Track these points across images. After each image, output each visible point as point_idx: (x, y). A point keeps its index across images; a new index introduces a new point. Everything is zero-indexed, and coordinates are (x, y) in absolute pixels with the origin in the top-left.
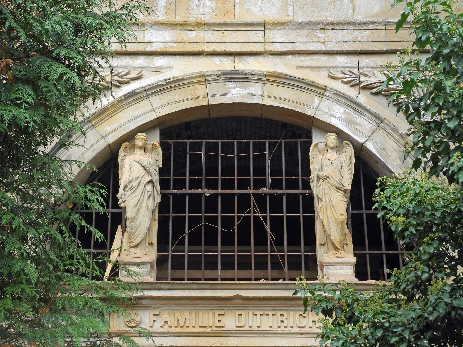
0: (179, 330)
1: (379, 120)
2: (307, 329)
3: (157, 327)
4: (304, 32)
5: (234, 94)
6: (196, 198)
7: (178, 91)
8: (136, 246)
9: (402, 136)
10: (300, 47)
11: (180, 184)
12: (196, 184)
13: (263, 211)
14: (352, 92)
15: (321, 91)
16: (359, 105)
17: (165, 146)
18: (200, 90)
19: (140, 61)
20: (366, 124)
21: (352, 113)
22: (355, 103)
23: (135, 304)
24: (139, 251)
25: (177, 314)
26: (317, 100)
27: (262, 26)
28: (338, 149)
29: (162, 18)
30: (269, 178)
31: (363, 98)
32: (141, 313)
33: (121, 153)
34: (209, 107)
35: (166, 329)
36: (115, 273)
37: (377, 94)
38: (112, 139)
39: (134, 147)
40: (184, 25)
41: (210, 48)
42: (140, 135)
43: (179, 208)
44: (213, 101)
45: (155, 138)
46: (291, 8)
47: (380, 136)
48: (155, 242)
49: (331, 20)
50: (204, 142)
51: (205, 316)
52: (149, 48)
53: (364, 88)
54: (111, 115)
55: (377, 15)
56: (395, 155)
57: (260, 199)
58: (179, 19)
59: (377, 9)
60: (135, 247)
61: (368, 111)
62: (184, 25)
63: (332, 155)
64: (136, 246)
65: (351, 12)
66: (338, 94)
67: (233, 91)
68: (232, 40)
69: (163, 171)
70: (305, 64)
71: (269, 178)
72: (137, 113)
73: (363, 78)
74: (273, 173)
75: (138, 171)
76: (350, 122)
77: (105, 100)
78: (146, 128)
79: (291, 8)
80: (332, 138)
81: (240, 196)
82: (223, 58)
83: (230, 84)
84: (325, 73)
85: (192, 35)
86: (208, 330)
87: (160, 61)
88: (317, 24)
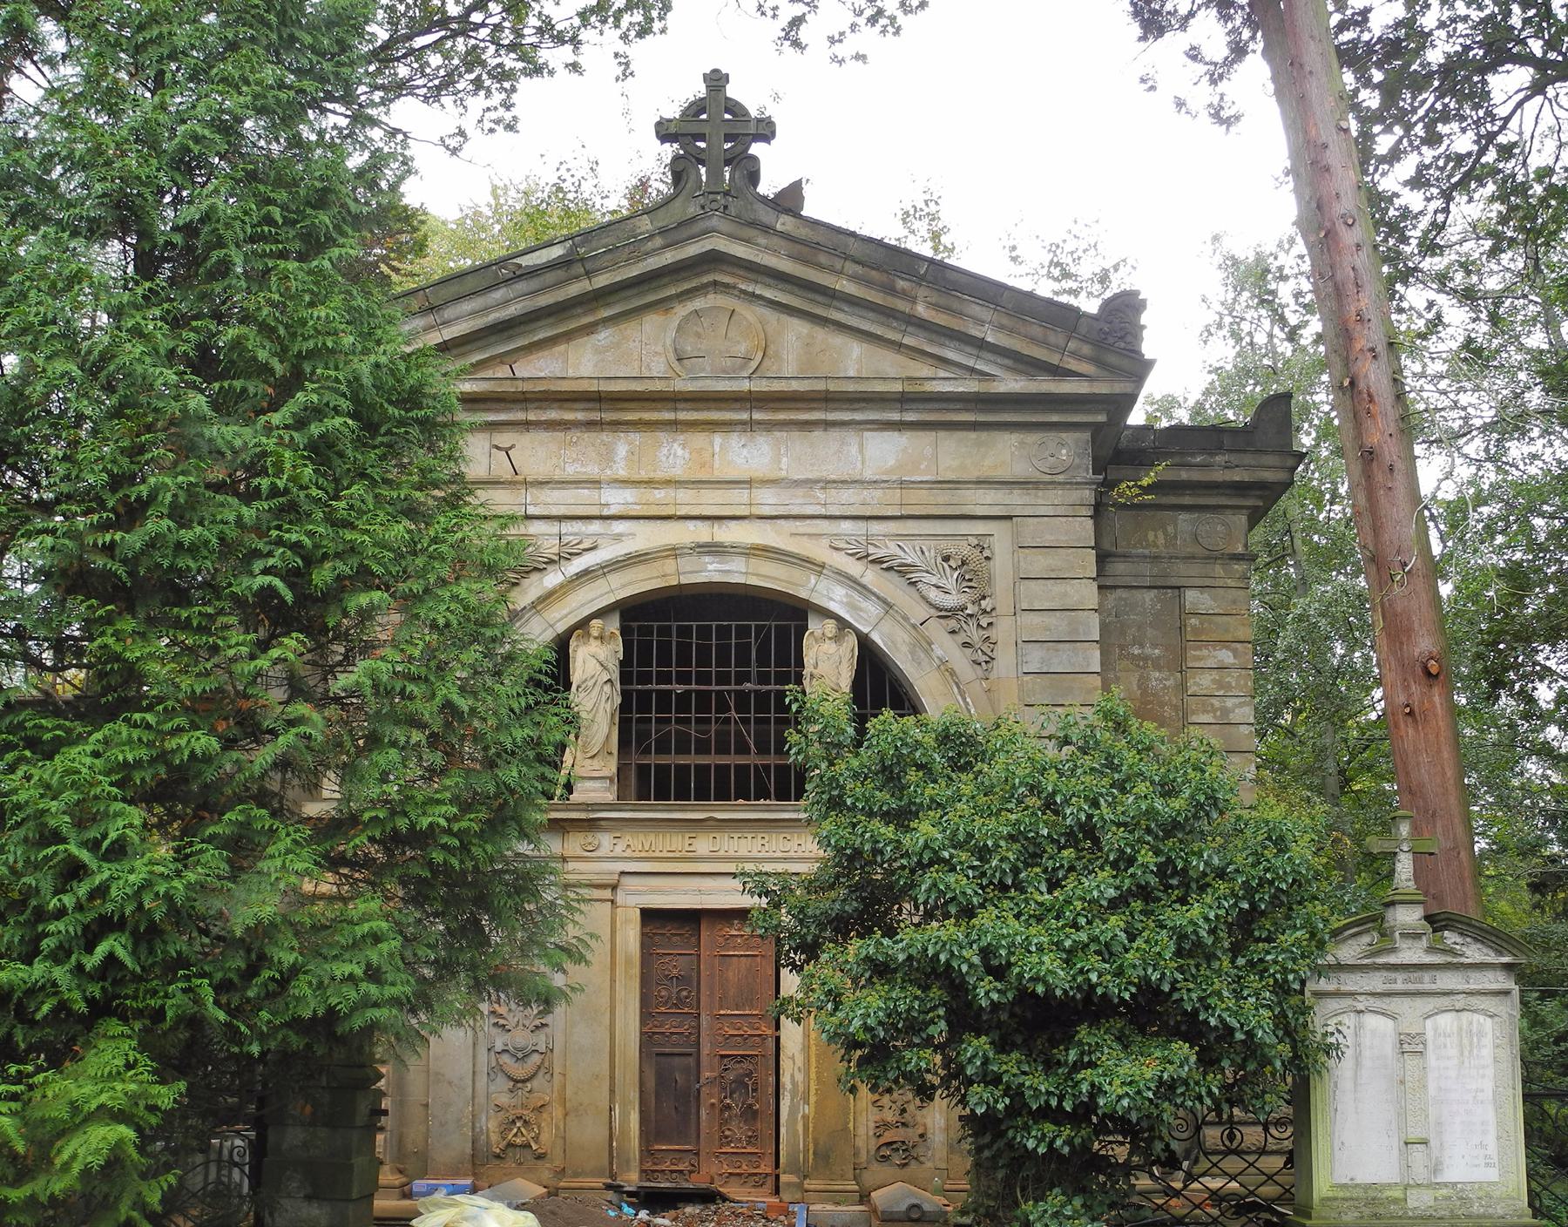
0: (643, 854)
1: (888, 605)
2: (792, 854)
3: (618, 851)
4: (800, 491)
5: (711, 571)
6: (664, 696)
7: (641, 567)
8: (593, 757)
9: (914, 626)
10: (795, 511)
11: (645, 678)
12: (664, 678)
13: (738, 733)
14: (855, 568)
15: (820, 567)
16: (864, 587)
17: (625, 631)
18: (669, 566)
19: (595, 527)
20: (872, 609)
21: (856, 596)
22: (859, 584)
23: (591, 825)
24: (596, 763)
25: (641, 837)
26: (813, 579)
27: (749, 483)
28: (837, 639)
29: (622, 473)
30: (754, 669)
31: (870, 576)
32: (599, 835)
33: (573, 643)
34: (680, 586)
35: (628, 853)
36: (569, 787)
37: (890, 569)
38: (561, 628)
39: (589, 635)
40: (649, 483)
41: (682, 512)
42: (595, 623)
43: (644, 706)
44: (684, 581)
45: (614, 625)
46: (785, 459)
47: (887, 626)
48: (615, 752)
49: (833, 477)
50: (674, 625)
51: (674, 838)
52: (606, 512)
53: (873, 562)
54: (559, 599)
55: (887, 472)
56: (905, 649)
57: (742, 698)
58: (644, 475)
59: (892, 462)
60: (592, 768)
61: (874, 594)
62: (649, 483)
63: (829, 647)
64: (593, 757)
65: (859, 465)
66: (839, 573)
67: (710, 567)
68: (711, 501)
69: (624, 664)
70: (801, 530)
71: (754, 669)
72: (591, 596)
73: (871, 550)
74: (760, 663)
75: (593, 667)
76: (853, 607)
77: (552, 579)
78: (601, 614)
79: (785, 459)
80: (830, 626)
81: (718, 693)
82: (699, 523)
83: (707, 559)
84: (825, 542)
85: (659, 494)
86: (677, 855)
87: (619, 527)
88: (817, 481)
